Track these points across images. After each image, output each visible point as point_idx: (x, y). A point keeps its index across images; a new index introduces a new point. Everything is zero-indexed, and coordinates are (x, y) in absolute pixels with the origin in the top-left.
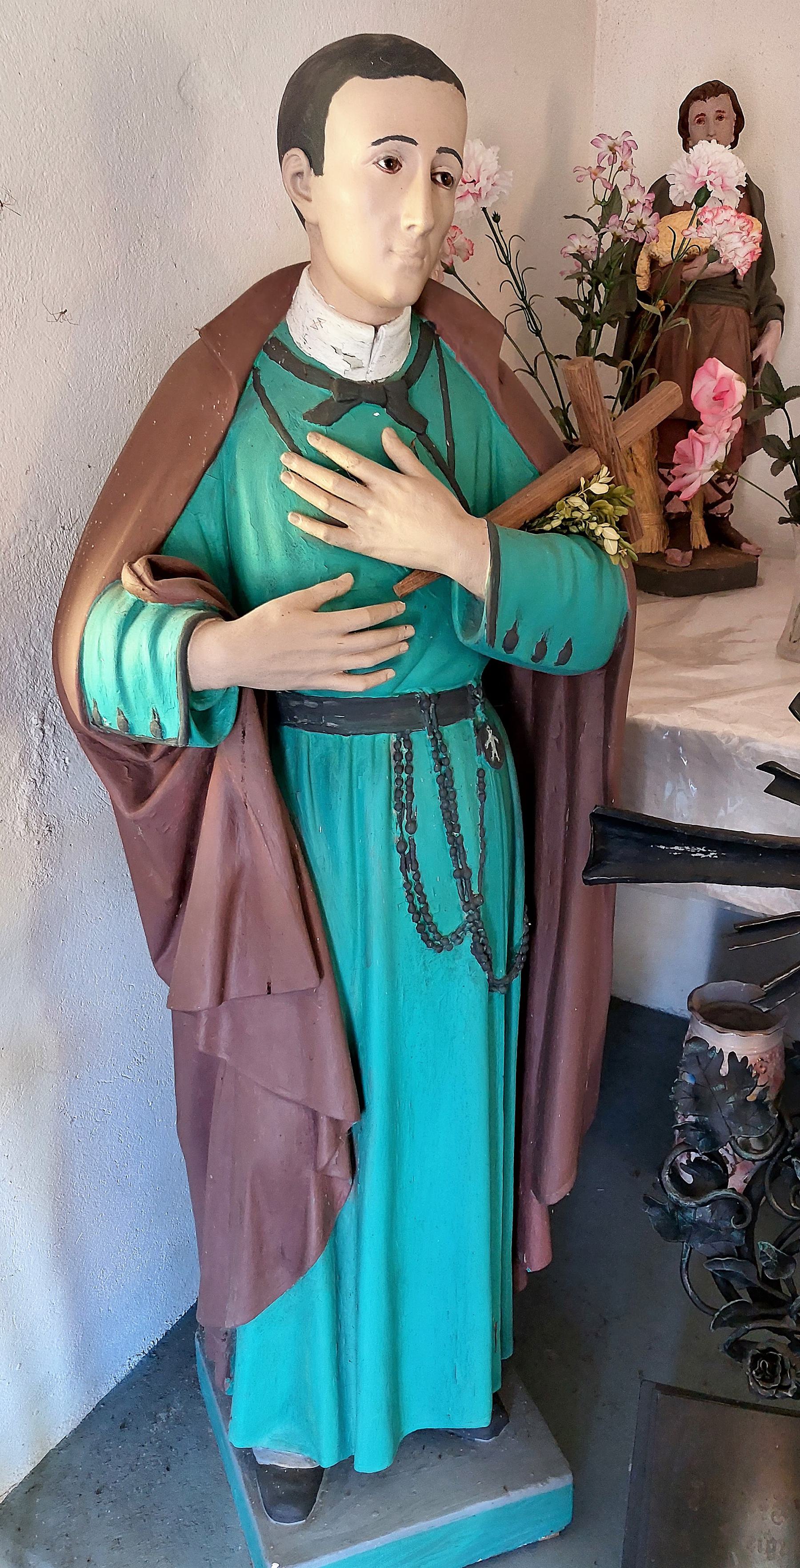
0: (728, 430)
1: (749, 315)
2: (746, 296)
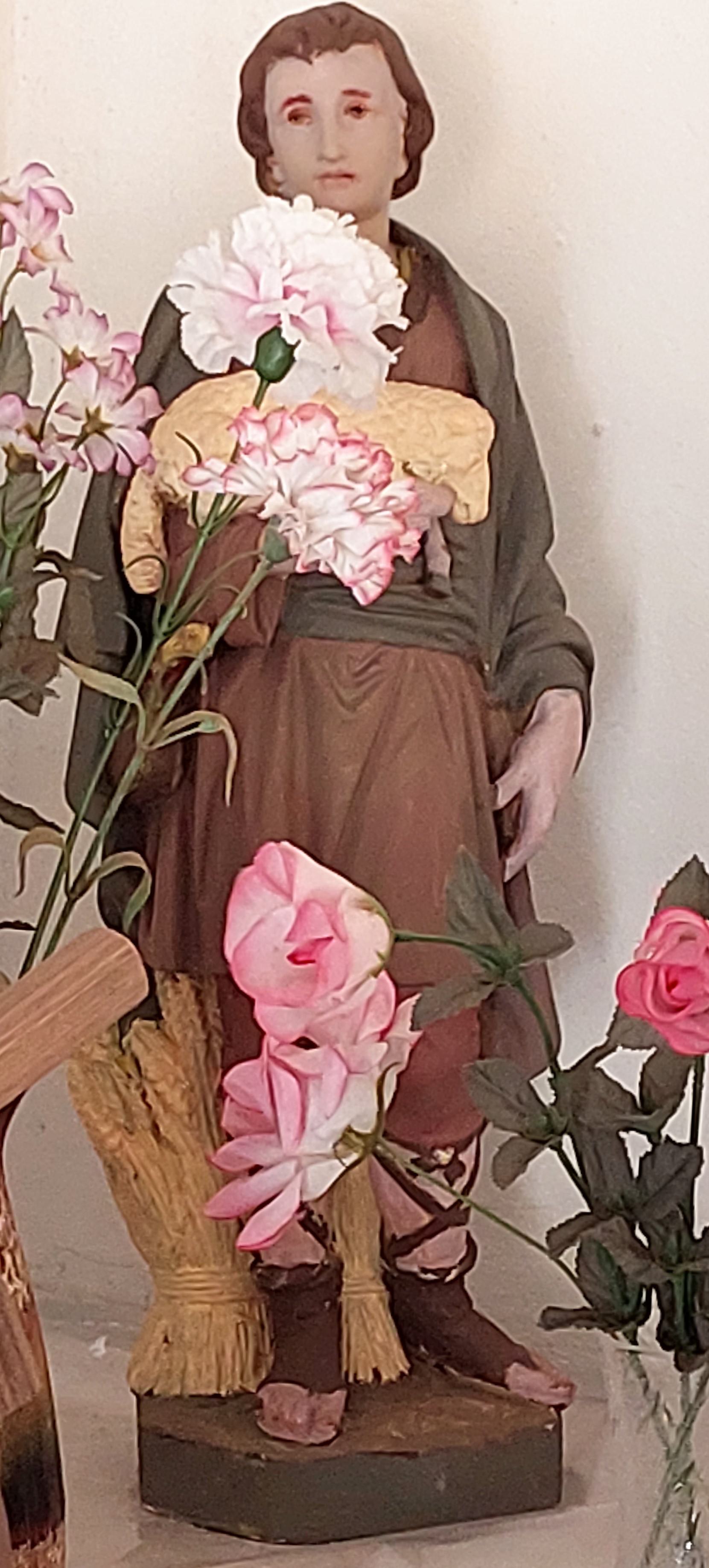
0: (383, 1035)
1: (481, 670)
2: (467, 621)
